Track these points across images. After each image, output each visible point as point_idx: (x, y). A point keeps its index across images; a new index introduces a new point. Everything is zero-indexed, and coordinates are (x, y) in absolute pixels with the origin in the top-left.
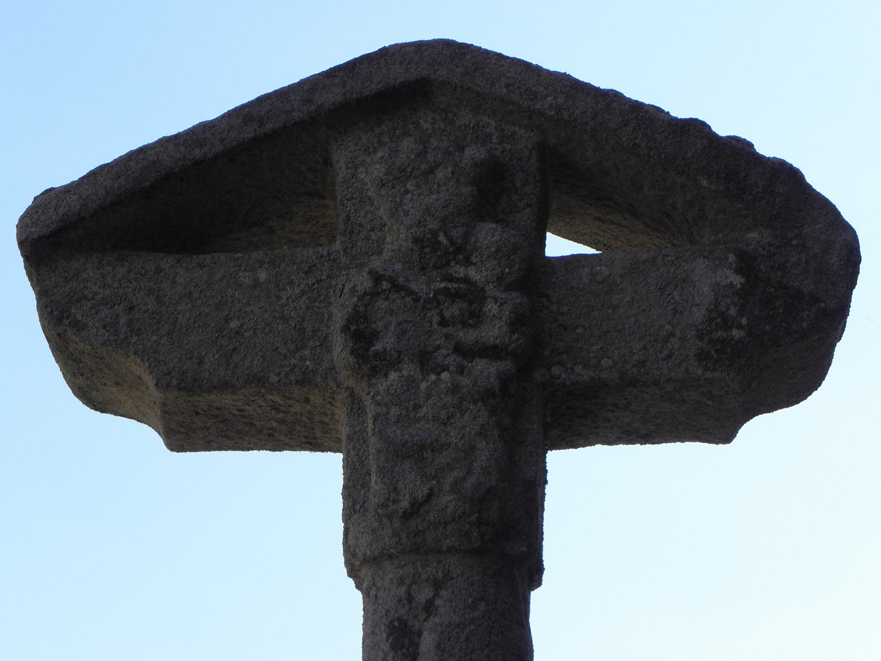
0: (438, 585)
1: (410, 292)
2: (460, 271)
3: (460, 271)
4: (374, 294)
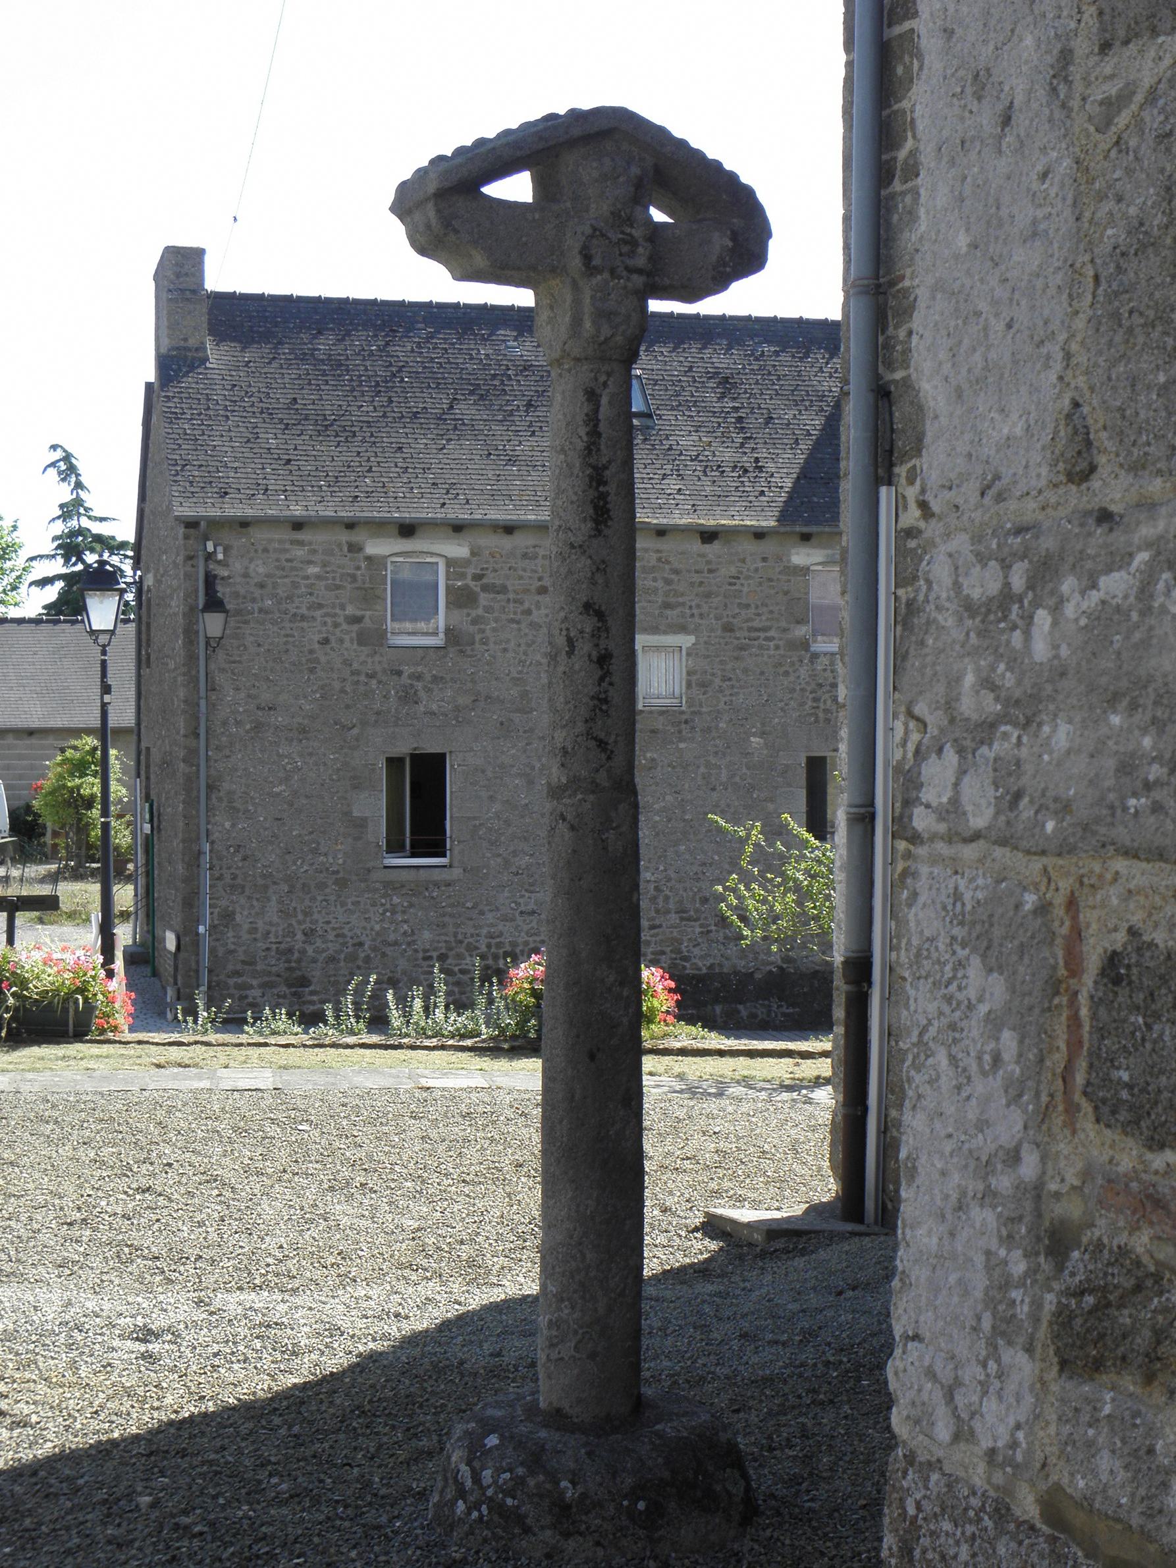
0: (609, 374)
1: (608, 238)
2: (628, 230)
3: (628, 230)
4: (592, 236)
